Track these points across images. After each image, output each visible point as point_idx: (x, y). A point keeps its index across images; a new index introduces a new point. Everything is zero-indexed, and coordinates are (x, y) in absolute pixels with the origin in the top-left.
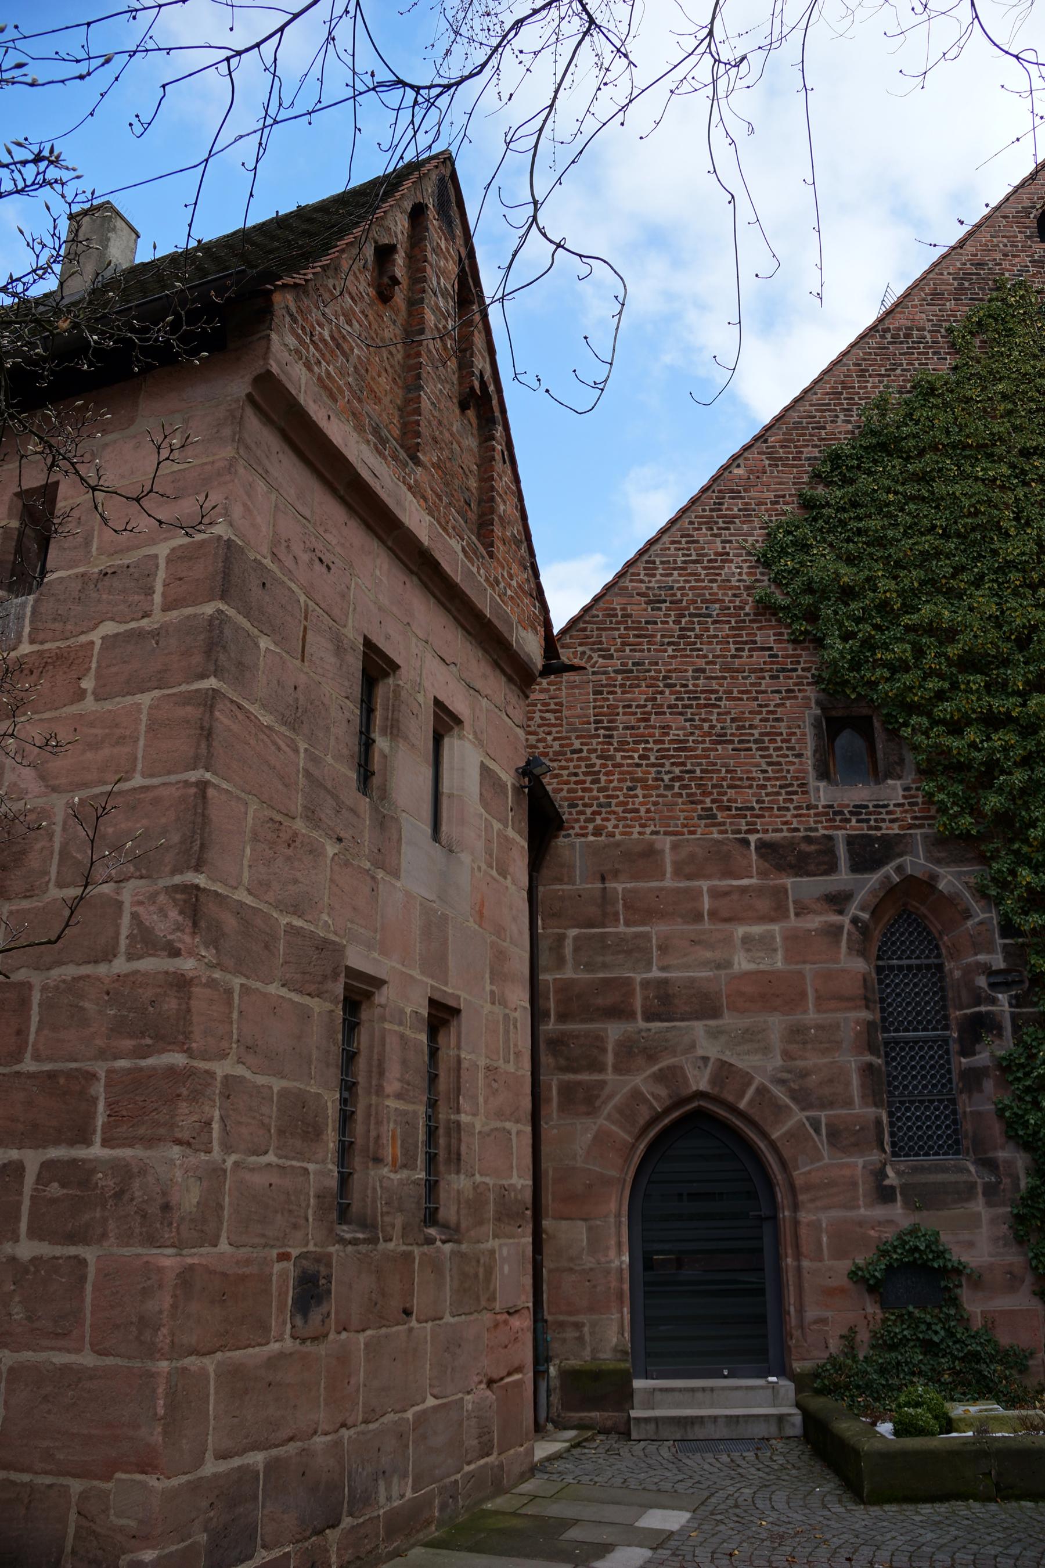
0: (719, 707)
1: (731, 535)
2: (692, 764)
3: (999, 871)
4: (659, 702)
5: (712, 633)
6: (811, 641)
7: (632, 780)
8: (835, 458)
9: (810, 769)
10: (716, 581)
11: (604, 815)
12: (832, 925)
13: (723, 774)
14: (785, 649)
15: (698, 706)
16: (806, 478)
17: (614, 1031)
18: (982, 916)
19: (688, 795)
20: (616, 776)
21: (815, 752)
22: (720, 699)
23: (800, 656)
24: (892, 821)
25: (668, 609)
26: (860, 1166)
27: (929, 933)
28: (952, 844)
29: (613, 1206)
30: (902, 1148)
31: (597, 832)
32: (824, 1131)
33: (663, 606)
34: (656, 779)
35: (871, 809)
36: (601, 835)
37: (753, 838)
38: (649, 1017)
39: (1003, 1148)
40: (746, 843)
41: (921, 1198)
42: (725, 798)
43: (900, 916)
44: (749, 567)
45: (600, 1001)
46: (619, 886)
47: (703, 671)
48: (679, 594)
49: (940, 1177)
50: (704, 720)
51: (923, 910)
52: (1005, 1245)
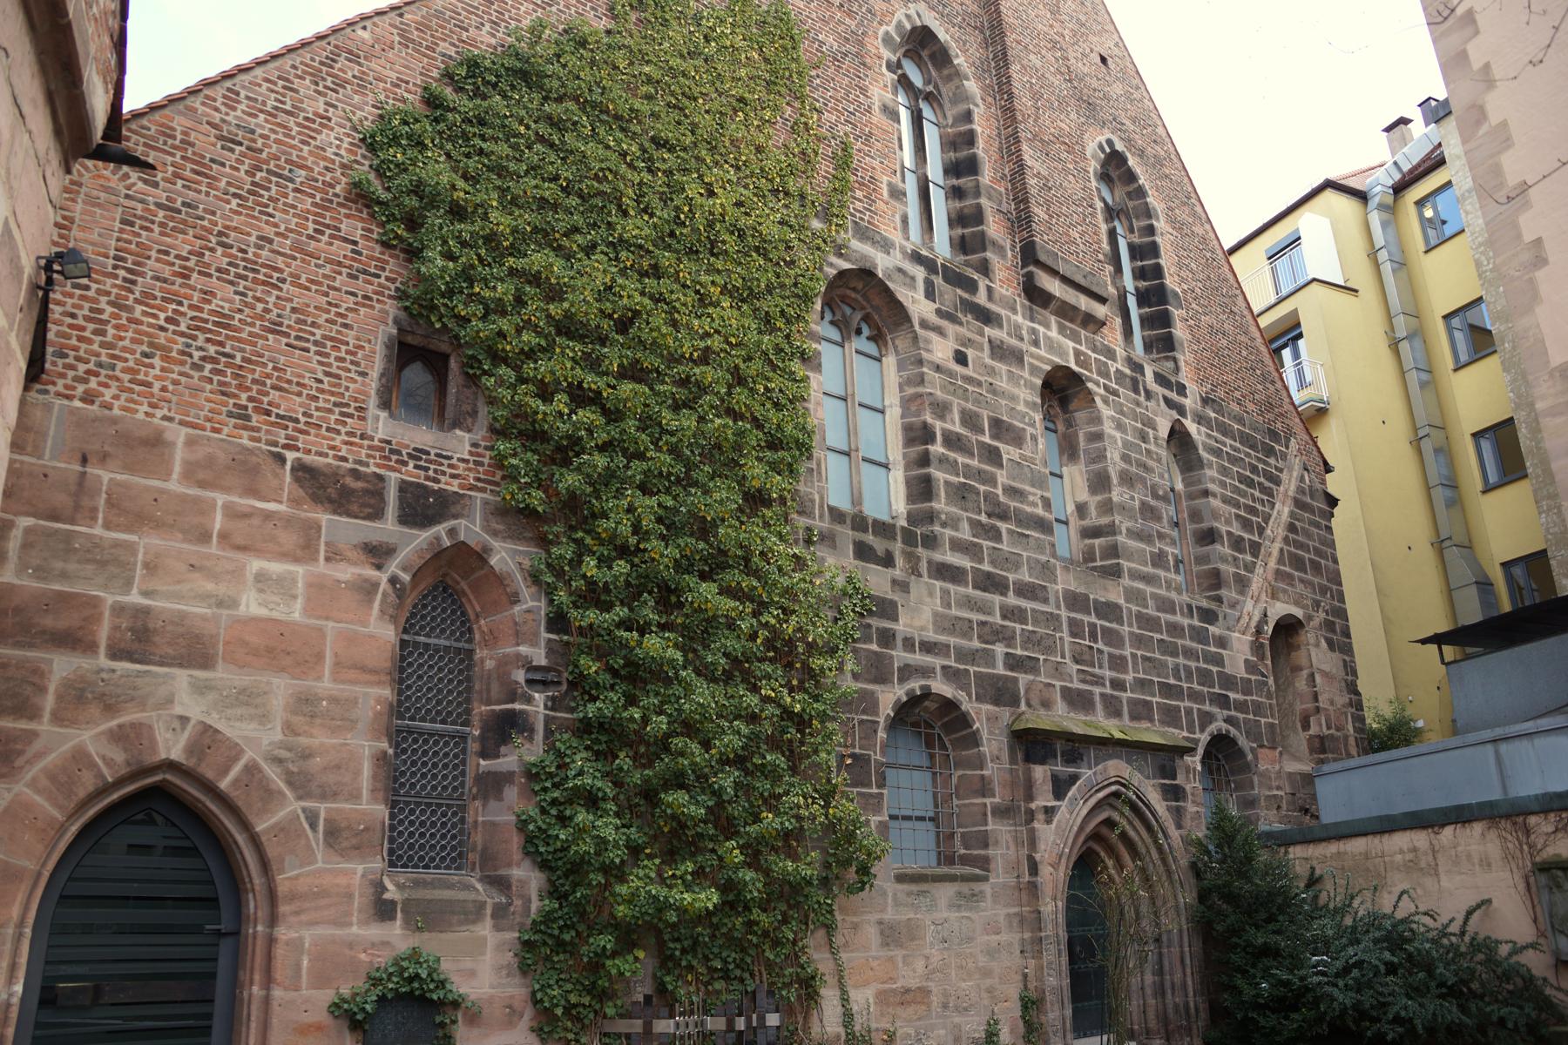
0: (281, 289)
1: (338, 100)
2: (233, 348)
3: (561, 557)
4: (206, 259)
5: (290, 201)
6: (403, 250)
7: (151, 345)
8: (473, 65)
9: (373, 393)
10: (309, 144)
11: (102, 379)
12: (366, 580)
13: (269, 370)
14: (373, 250)
15: (255, 281)
16: (435, 73)
17: (62, 666)
18: (531, 604)
19: (221, 383)
20: (130, 334)
21: (382, 375)
22: (283, 281)
23: (387, 262)
24: (453, 476)
25: (243, 154)
26: (360, 872)
27: (464, 614)
28: (518, 518)
29: (15, 912)
30: (400, 857)
31: (89, 398)
32: (321, 828)
33: (238, 148)
34: (183, 353)
35: (432, 457)
36: (92, 402)
37: (290, 456)
38: (116, 653)
39: (518, 865)
40: (281, 459)
41: (425, 917)
42: (266, 400)
43: (435, 588)
44: (351, 144)
45: (48, 622)
46: (104, 476)
47: (271, 241)
48: (260, 141)
49: (447, 894)
50: (259, 300)
51: (464, 585)
52: (508, 975)
